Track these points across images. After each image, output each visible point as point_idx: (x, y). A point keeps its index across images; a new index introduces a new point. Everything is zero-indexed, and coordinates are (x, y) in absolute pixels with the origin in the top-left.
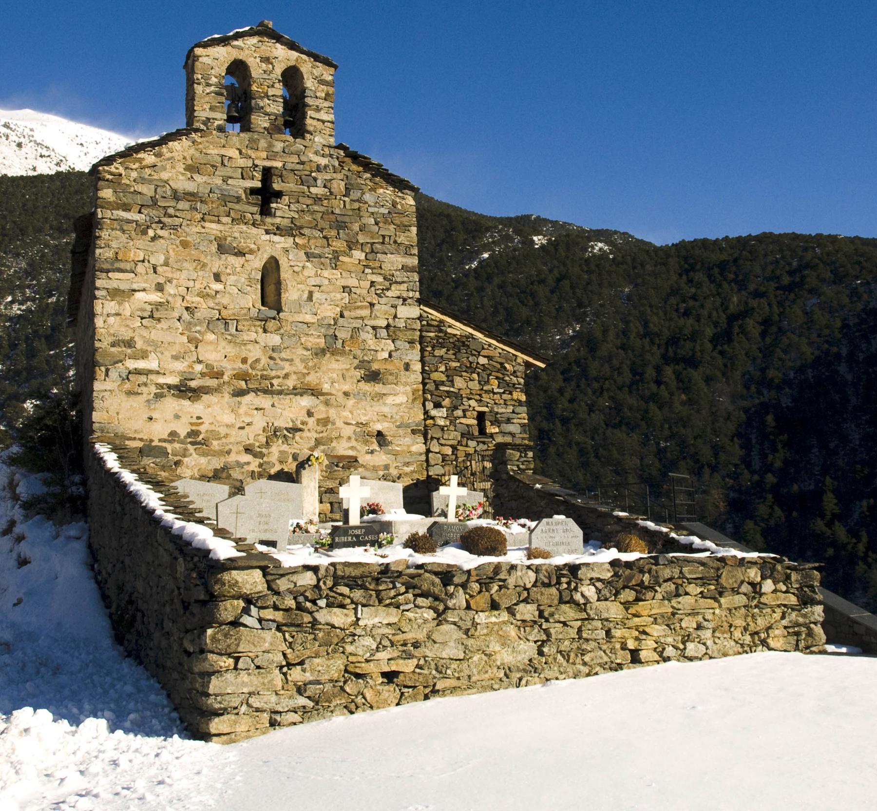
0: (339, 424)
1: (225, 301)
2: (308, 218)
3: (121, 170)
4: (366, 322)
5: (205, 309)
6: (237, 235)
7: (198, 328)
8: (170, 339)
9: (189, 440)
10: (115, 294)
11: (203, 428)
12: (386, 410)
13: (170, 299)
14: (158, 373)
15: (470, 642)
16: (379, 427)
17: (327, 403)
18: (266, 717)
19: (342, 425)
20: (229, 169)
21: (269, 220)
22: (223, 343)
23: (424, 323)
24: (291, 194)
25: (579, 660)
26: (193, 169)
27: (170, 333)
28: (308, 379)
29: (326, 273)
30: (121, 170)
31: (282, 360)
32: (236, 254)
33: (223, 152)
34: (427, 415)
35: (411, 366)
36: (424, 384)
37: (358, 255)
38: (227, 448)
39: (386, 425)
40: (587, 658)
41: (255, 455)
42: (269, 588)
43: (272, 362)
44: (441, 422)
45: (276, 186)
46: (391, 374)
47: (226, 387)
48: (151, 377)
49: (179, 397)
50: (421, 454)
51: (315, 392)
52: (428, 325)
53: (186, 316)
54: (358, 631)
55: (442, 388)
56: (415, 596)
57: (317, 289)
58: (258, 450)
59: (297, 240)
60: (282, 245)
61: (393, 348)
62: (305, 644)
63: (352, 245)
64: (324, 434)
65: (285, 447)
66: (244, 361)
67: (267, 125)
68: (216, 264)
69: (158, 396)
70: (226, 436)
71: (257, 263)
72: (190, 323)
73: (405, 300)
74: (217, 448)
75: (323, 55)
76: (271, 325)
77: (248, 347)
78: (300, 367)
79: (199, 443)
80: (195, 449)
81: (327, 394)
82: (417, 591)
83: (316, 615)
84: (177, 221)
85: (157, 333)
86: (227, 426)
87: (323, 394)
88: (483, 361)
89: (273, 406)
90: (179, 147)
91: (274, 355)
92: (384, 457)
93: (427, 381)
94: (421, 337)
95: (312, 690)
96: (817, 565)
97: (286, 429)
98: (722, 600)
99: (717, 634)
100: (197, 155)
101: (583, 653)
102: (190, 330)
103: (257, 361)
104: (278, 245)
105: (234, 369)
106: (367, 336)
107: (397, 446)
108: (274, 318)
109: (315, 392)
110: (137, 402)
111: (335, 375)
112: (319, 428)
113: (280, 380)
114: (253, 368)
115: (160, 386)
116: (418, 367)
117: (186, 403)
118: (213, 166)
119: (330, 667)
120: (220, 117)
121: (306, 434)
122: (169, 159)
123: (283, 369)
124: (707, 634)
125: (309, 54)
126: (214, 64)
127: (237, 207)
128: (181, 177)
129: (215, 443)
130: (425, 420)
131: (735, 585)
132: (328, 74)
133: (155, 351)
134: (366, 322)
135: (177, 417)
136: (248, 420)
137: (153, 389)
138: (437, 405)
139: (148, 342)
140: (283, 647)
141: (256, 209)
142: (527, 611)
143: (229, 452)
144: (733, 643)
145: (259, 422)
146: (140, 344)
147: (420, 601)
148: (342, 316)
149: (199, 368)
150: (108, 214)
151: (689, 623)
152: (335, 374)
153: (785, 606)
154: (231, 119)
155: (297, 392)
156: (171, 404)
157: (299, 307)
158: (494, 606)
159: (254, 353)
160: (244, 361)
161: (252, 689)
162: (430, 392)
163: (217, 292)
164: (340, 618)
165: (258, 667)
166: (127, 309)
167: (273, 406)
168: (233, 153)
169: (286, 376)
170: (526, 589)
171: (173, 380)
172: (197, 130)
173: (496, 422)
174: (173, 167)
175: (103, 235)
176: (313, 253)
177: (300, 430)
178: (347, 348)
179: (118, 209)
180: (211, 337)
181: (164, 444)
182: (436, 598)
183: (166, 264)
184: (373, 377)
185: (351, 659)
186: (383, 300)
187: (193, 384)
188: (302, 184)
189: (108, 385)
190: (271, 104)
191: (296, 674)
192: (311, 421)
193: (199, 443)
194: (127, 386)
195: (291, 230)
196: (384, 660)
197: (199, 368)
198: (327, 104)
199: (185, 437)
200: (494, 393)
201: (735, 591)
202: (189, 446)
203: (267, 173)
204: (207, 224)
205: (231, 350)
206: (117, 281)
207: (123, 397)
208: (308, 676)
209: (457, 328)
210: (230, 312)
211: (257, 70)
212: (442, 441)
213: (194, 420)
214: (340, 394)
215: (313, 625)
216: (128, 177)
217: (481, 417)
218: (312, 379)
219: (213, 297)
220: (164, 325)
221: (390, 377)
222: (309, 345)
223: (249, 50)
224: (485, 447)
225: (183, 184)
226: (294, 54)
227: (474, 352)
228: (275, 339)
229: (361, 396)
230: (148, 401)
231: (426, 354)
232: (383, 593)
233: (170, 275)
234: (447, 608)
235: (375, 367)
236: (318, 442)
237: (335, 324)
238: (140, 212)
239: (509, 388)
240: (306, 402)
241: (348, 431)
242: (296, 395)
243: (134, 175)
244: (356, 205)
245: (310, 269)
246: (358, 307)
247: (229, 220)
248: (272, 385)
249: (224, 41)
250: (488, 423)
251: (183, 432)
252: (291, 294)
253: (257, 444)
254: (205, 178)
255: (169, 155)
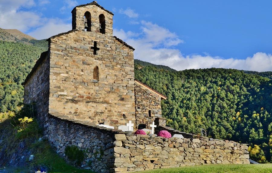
0: (114, 112)
1: (84, 77)
2: (106, 56)
3: (57, 40)
4: (121, 85)
5: (79, 79)
6: (87, 59)
7: (77, 84)
8: (70, 87)
9: (75, 114)
11: (78, 111)
12: (126, 108)
13: (70, 76)
14: (67, 96)
15: (169, 155)
16: (124, 113)
17: (110, 106)
18: (127, 168)
19: (114, 112)
20: (86, 42)
21: (96, 56)
22: (84, 88)
23: (136, 86)
24: (102, 49)
25: (193, 161)
26: (76, 41)
28: (106, 99)
29: (110, 71)
30: (57, 40)
31: (99, 94)
32: (87, 65)
33: (84, 36)
34: (136, 111)
35: (132, 97)
36: (135, 102)
37: (119, 66)
38: (84, 117)
39: (126, 112)
40: (195, 161)
41: (92, 119)
42: (127, 139)
43: (96, 94)
44: (140, 113)
45: (98, 47)
46: (127, 99)
47: (84, 100)
48: (65, 97)
49: (72, 102)
50: (135, 121)
51: (107, 102)
52: (137, 86)
53: (74, 81)
54: (145, 150)
55: (140, 103)
56: (157, 143)
58: (93, 118)
59: (103, 62)
60: (99, 63)
61: (128, 92)
62: (135, 153)
63: (117, 63)
64: (110, 114)
65: (99, 117)
66: (89, 93)
67: (95, 30)
68: (82, 67)
69: (67, 102)
70: (84, 114)
71: (93, 67)
72: (75, 83)
73: (131, 79)
74: (82, 117)
75: (110, 11)
76: (96, 84)
77: (90, 90)
78: (104, 96)
79: (77, 115)
80: (76, 117)
81: (111, 104)
82: (158, 142)
83: (137, 146)
84: (72, 55)
85: (67, 84)
86: (85, 111)
87: (110, 103)
88: (150, 97)
89: (96, 106)
90: (72, 34)
91: (97, 92)
92: (125, 121)
93: (136, 101)
94: (135, 89)
95: (136, 163)
96: (247, 144)
97: (100, 112)
98: (225, 150)
99: (224, 158)
100: (77, 37)
101: (194, 160)
102: (75, 85)
103: (93, 94)
104: (98, 63)
105: (86, 96)
106: (121, 89)
107: (129, 118)
108: (97, 82)
109: (107, 102)
110: (61, 103)
111: (113, 99)
112: (108, 113)
113: (99, 99)
114: (92, 96)
115: (67, 99)
116: (134, 97)
117: (74, 104)
118: (81, 40)
119: (140, 158)
120: (83, 27)
121: (105, 114)
122: (70, 38)
123: (99, 96)
124: (222, 158)
125: (106, 11)
126: (81, 12)
127: (87, 52)
128: (73, 43)
129: (81, 115)
130: (136, 112)
131: (228, 147)
132: (111, 16)
133: (66, 90)
134: (121, 85)
135: (71, 108)
136: (90, 109)
137: (65, 100)
138: (139, 108)
139: (64, 87)
140: (130, 153)
141: (93, 53)
142: (182, 149)
143: (85, 118)
144: (228, 161)
145: (93, 110)
146: (62, 88)
147: (158, 144)
148: (114, 83)
149: (77, 95)
150: (53, 52)
151: (218, 155)
152: (113, 98)
153: (240, 153)
154: (86, 28)
155: (102, 103)
156: (70, 104)
157: (103, 80)
158: (174, 147)
159: (92, 91)
160: (89, 93)
161: (124, 162)
163: (82, 75)
164: (142, 147)
165: (125, 157)
166: (59, 78)
167: (96, 106)
168: (86, 37)
169: (100, 98)
170: (181, 143)
171: (70, 98)
172: (77, 30)
173: (154, 113)
174: (71, 40)
175: (52, 58)
176: (107, 65)
177: (104, 113)
178: (116, 91)
179: (56, 51)
180: (81, 87)
181: (68, 115)
182: (162, 144)
183: (69, 66)
184: (122, 99)
185: (144, 156)
186: (125, 79)
187: (76, 99)
188: (104, 46)
189: (53, 99)
190: (96, 24)
191: (133, 159)
192: (106, 111)
193: (77, 115)
194: (58, 99)
195: (101, 59)
196: (151, 158)
197: (77, 95)
198: (111, 25)
199: (73, 114)
200: (153, 106)
201: (228, 148)
202: (74, 116)
203: (95, 43)
204: (80, 56)
205: (86, 90)
207: (57, 102)
208: (135, 160)
209: (144, 87)
210: (86, 80)
211: (92, 15)
212: (140, 118)
213: (76, 109)
214: (114, 104)
215: (136, 148)
216: (59, 42)
217: (150, 112)
219: (81, 76)
220: (68, 83)
221: (127, 100)
222: (106, 90)
223: (90, 9)
224: (151, 120)
225: (73, 45)
226: (103, 10)
227: (148, 94)
228: (97, 88)
229: (119, 104)
230: (64, 103)
231: (136, 94)
232: (151, 142)
233: (70, 69)
234: (164, 146)
235: (123, 97)
236: (108, 116)
237: (113, 85)
238: (62, 52)
239: (157, 104)
240: (105, 105)
241: (116, 114)
242: (102, 103)
243: (60, 41)
244: (118, 53)
245: (106, 70)
246: (119, 81)
247: (85, 55)
248: (96, 100)
250: (151, 114)
251: (73, 112)
252: (101, 76)
253: (92, 116)
254: (79, 43)
255: (69, 37)
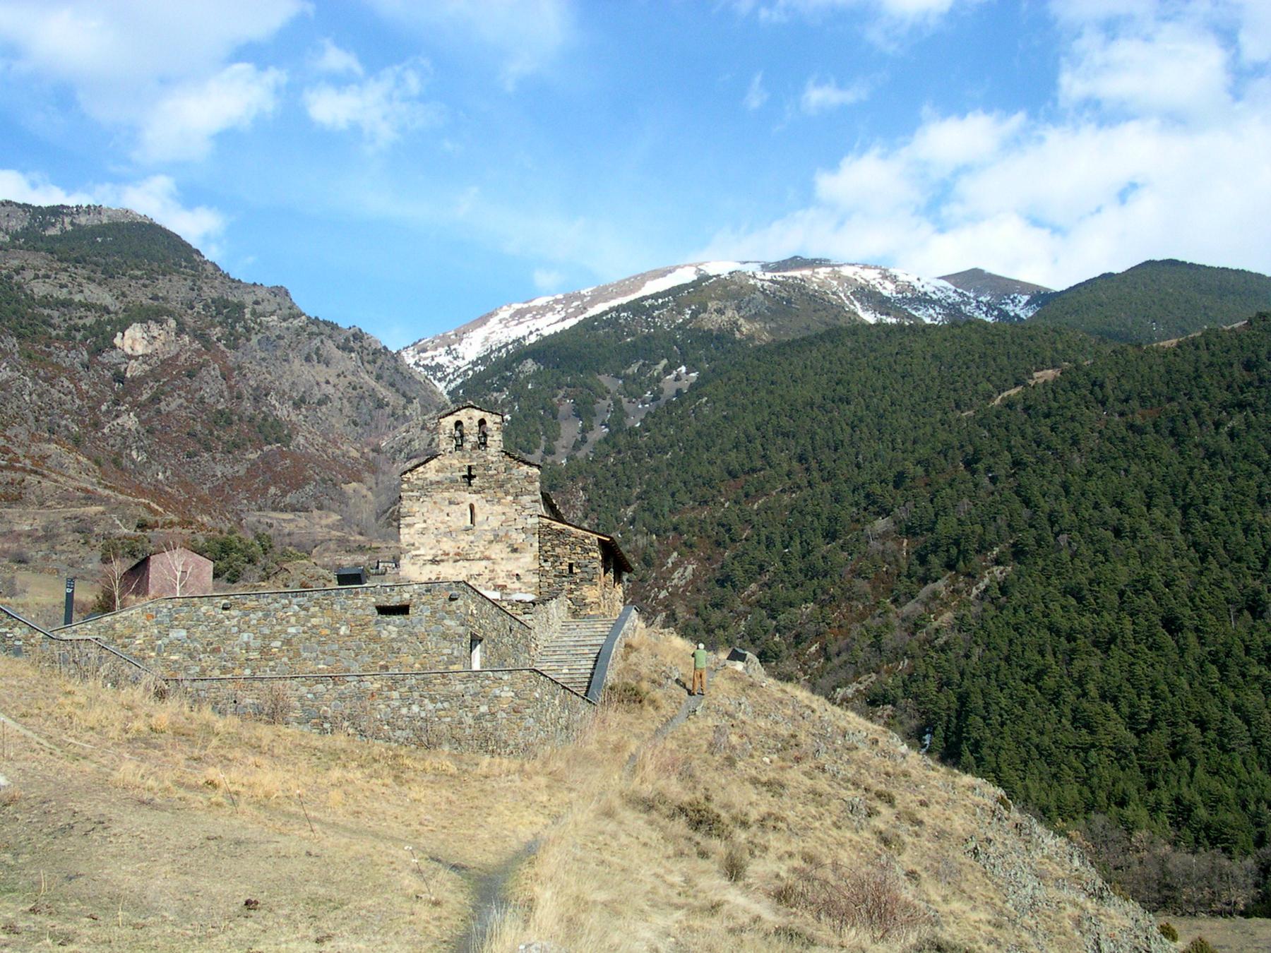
5: (443, 528)
10: (408, 526)
27: (429, 539)
37: (510, 498)
51: (488, 558)
57: (491, 514)
63: (507, 493)
68: (447, 509)
85: (424, 539)
109: (488, 558)
110: (416, 567)
116: (537, 545)
155: (480, 559)
156: (429, 567)
159: (463, 544)
162: (543, 556)
166: (412, 531)
168: (455, 462)
184: (515, 550)
203: (470, 468)
205: (453, 544)
206: (408, 520)
211: (466, 422)
217: (571, 566)
218: (487, 553)
228: (472, 538)
240: (484, 563)
249: (451, 413)
